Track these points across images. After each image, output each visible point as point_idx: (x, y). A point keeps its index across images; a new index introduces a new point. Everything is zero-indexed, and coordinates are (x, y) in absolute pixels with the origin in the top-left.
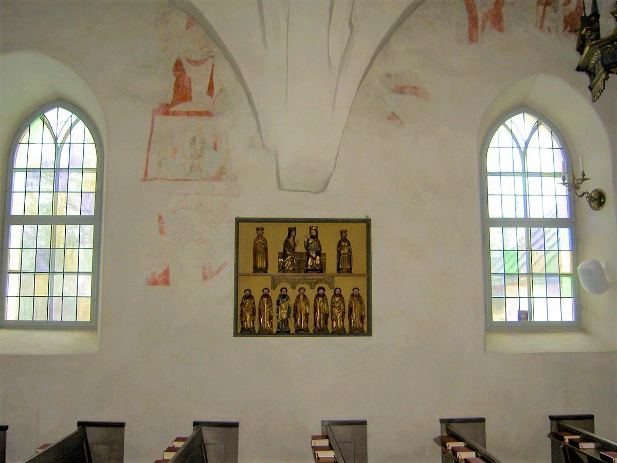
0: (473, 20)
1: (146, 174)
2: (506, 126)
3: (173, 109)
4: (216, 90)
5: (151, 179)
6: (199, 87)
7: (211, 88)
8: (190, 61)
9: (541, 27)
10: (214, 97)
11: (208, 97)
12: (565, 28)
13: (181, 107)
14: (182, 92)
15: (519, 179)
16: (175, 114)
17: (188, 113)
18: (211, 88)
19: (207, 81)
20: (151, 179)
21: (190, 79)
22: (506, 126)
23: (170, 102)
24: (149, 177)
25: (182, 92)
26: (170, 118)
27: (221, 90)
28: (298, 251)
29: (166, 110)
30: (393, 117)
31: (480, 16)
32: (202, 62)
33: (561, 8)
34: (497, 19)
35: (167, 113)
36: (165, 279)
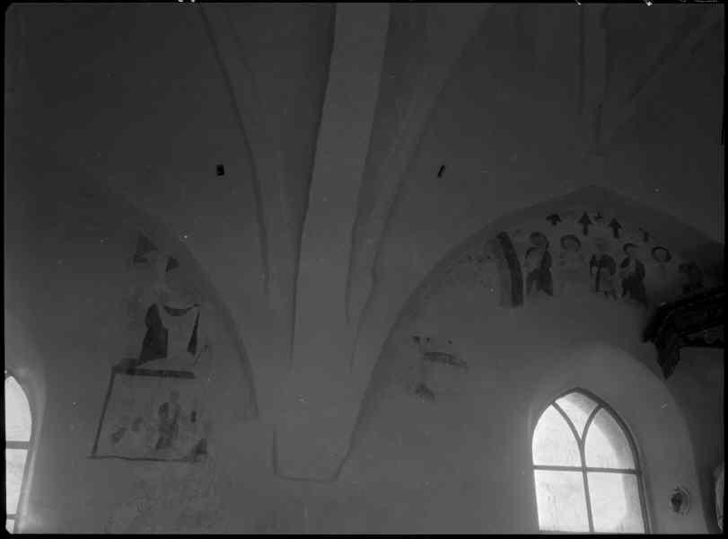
0: (517, 282)
1: (95, 447)
2: (557, 407)
3: (143, 366)
4: (199, 346)
5: (102, 457)
6: (177, 345)
7: (193, 342)
8: (167, 308)
9: (597, 290)
10: (196, 356)
11: (189, 355)
12: (625, 293)
13: (154, 365)
14: (155, 344)
15: (588, 465)
16: (144, 373)
17: (160, 373)
18: (193, 342)
19: (190, 335)
20: (102, 457)
21: (166, 332)
22: (557, 407)
23: (136, 356)
24: (100, 452)
25: (155, 344)
26: (137, 378)
27: (206, 346)
28: (23, 450)
29: (131, 369)
30: (423, 390)
31: (525, 275)
32: (185, 311)
33: (618, 270)
34: (543, 279)
35: (131, 372)
36: (221, 170)
